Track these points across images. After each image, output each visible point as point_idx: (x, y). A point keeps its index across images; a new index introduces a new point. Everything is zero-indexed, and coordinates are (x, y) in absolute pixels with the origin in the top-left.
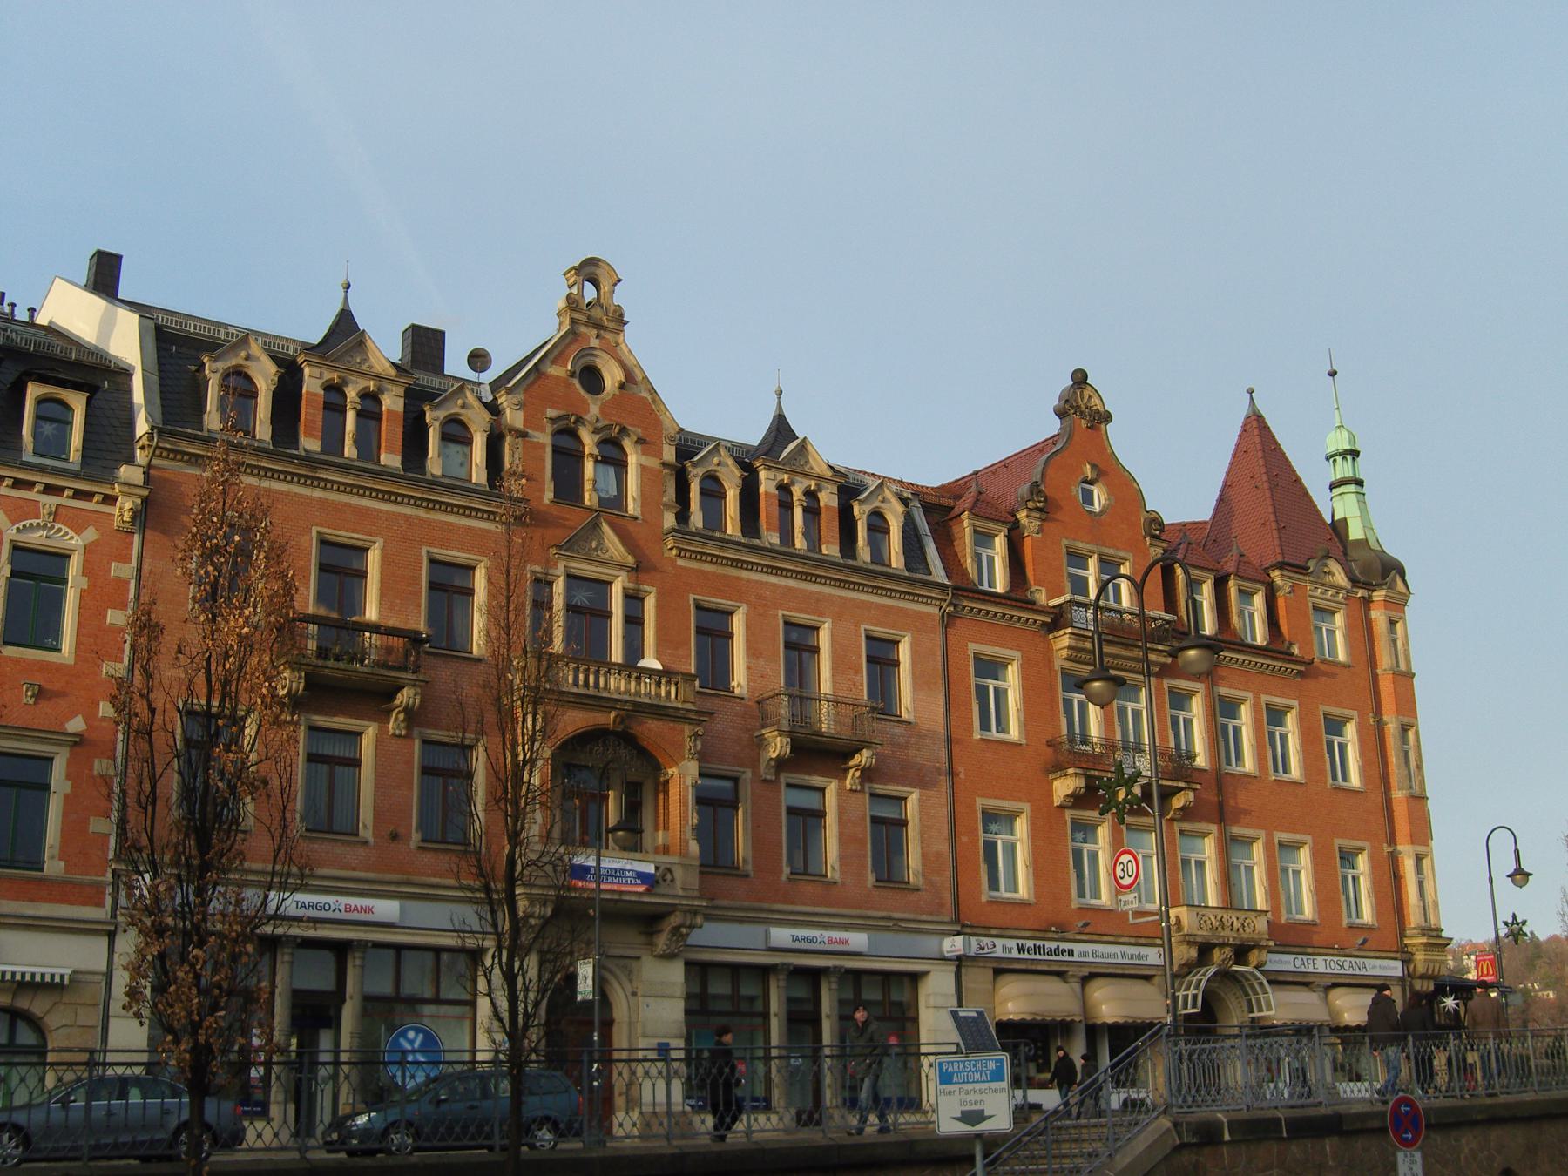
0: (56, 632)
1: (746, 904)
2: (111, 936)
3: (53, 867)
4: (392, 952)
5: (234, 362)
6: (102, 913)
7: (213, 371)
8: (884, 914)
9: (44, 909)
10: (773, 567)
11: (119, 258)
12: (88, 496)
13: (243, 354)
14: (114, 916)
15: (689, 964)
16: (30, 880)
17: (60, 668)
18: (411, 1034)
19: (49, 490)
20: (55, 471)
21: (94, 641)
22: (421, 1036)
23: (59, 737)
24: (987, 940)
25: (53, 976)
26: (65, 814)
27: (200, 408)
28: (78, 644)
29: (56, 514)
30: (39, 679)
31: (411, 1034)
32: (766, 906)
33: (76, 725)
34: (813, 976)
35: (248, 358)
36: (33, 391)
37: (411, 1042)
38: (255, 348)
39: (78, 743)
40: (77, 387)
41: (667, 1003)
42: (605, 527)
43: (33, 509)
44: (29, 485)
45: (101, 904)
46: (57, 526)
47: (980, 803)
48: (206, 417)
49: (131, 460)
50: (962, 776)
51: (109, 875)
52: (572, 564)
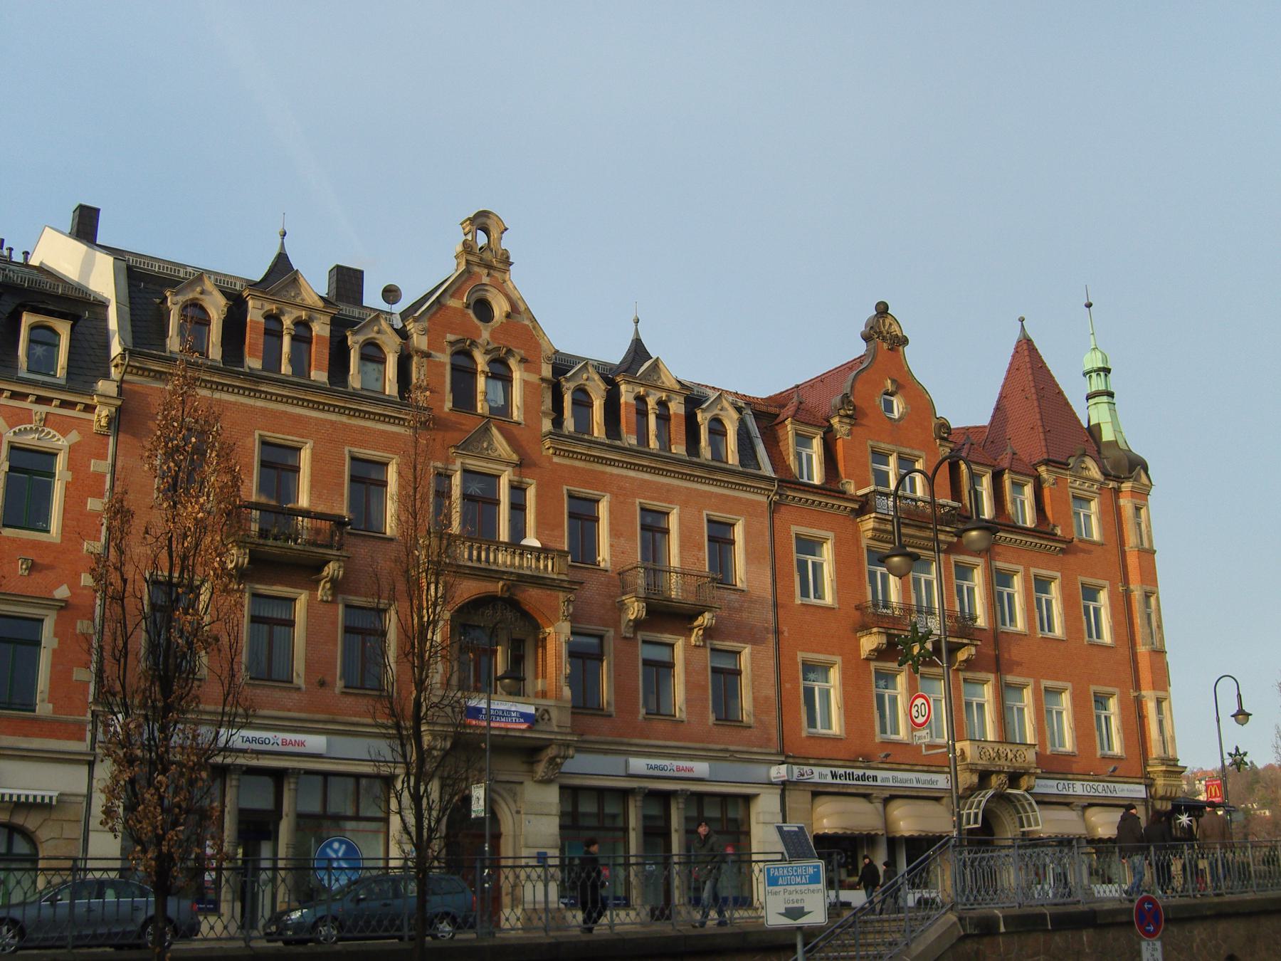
0: (46, 517)
1: (610, 739)
2: (91, 765)
3: (44, 708)
4: (320, 778)
5: (191, 296)
6: (84, 746)
7: (174, 304)
8: (722, 747)
9: (36, 743)
10: (631, 464)
11: (98, 211)
12: (72, 405)
13: (198, 289)
14: (93, 748)
15: (563, 788)
16: (24, 719)
17: (49, 546)
18: (336, 845)
19: (40, 400)
20: (45, 385)
21: (77, 524)
22: (344, 847)
23: (48, 602)
24: (806, 768)
25: (43, 797)
26: (53, 665)
27: (164, 333)
28: (64, 526)
29: (46, 420)
30: (32, 555)
31: (336, 845)
32: (626, 740)
33: (62, 592)
34: (664, 798)
35: (202, 292)
36: (27, 319)
37: (336, 851)
38: (208, 284)
39: (64, 607)
40: (63, 316)
41: (545, 819)
42: (494, 430)
43: (27, 416)
44: (24, 396)
45: (82, 739)
46: (47, 430)
47: (801, 656)
48: (168, 341)
49: (107, 376)
50: (786, 634)
51: (89, 715)
52: (467, 461)
